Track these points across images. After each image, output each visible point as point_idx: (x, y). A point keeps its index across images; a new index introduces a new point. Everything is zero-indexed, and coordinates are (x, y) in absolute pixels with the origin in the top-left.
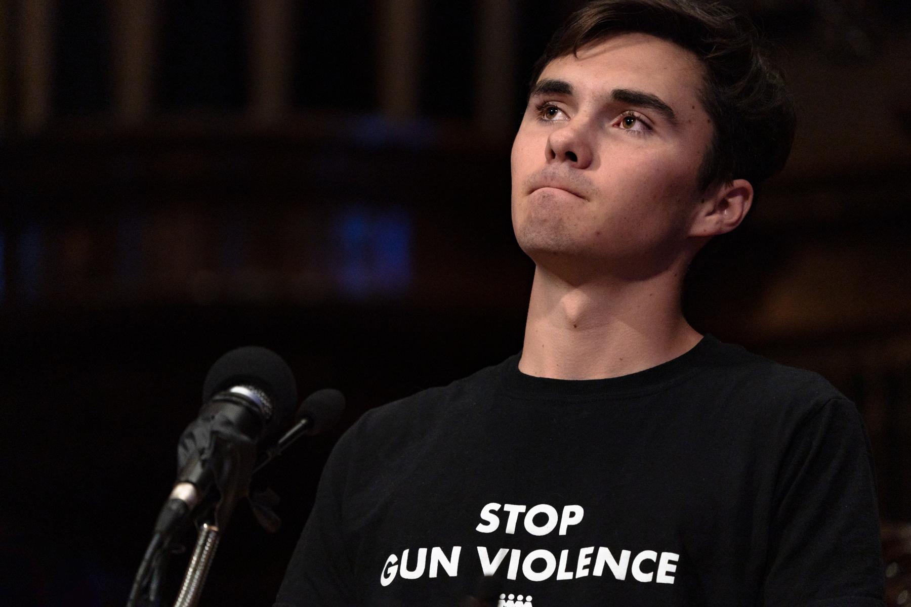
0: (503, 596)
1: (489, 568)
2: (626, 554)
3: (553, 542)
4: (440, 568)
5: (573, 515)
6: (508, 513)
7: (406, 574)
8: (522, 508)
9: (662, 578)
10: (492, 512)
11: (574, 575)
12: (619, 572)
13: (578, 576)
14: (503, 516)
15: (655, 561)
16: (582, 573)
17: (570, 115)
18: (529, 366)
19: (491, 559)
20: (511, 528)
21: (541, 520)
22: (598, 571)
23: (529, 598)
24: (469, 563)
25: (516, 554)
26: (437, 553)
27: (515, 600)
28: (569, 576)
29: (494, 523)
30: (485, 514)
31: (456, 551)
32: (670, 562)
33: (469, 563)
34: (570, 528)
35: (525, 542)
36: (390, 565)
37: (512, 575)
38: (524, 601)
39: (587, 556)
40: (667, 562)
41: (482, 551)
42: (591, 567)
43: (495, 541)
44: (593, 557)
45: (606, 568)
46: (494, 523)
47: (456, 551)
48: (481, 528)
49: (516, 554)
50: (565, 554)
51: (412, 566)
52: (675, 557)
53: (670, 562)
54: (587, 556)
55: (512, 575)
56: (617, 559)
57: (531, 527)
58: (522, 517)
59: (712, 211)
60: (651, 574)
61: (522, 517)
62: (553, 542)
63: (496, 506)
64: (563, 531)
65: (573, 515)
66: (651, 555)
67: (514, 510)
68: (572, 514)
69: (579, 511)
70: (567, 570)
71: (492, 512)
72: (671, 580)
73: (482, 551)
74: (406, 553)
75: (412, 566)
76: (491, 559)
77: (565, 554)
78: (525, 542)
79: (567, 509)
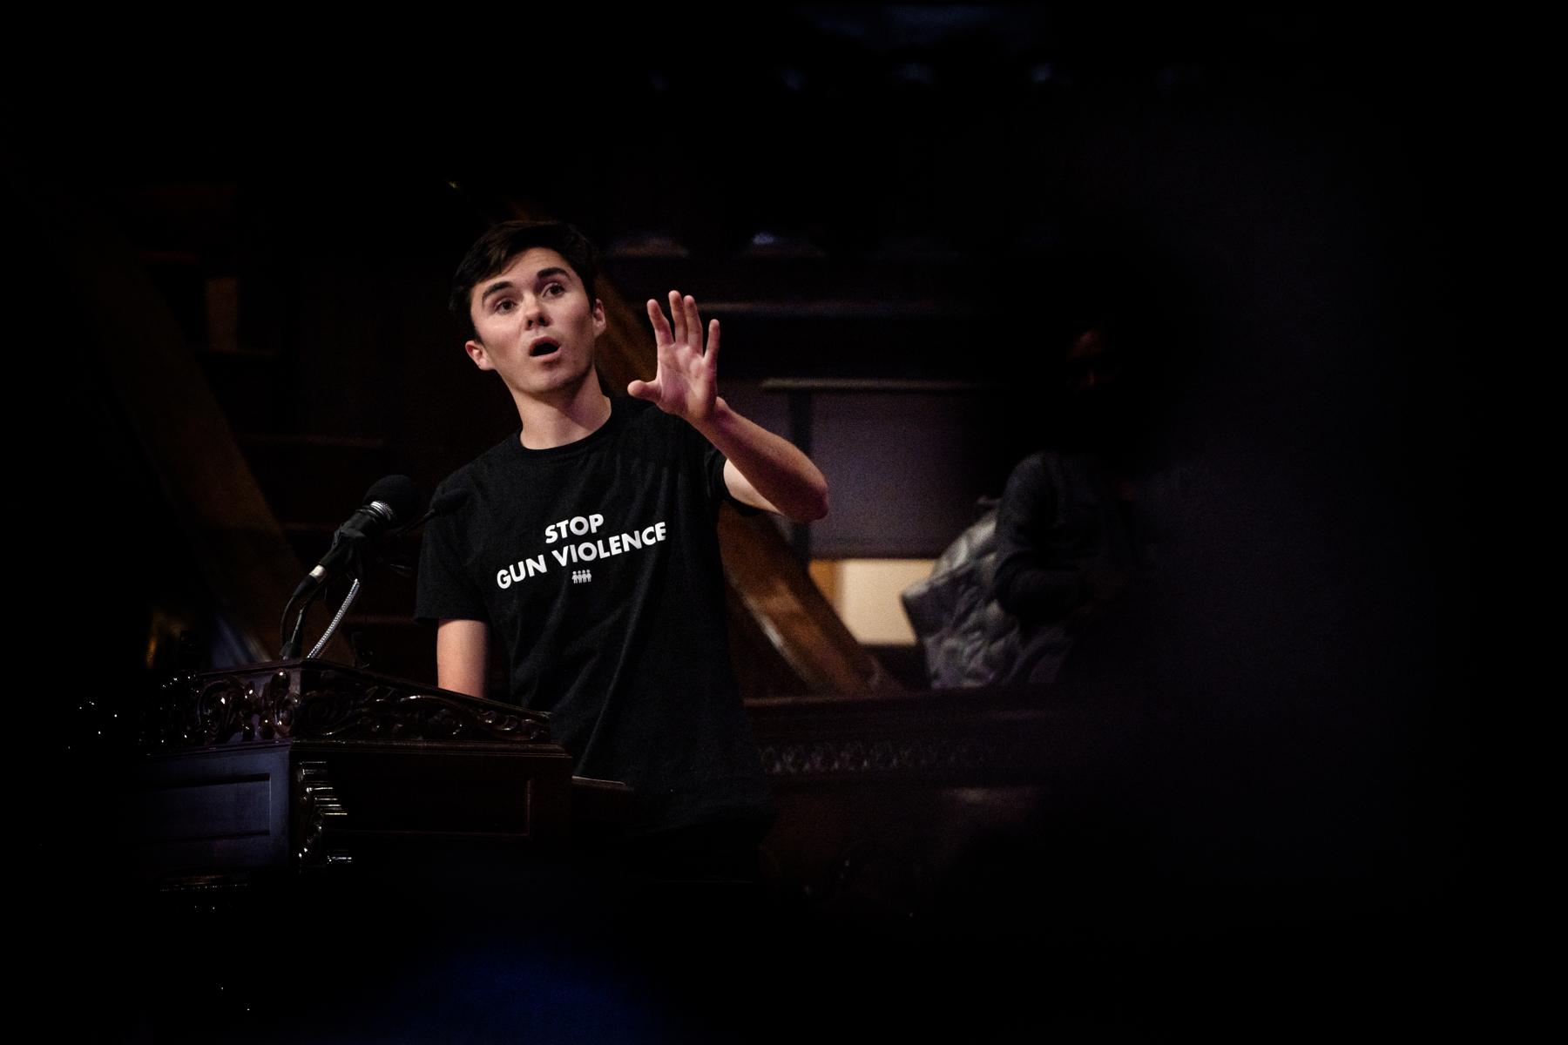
0: (574, 573)
1: (563, 561)
3: (590, 537)
4: (634, 537)
5: (597, 520)
6: (560, 528)
7: (517, 579)
8: (566, 522)
9: (660, 538)
11: (656, 539)
12: (638, 545)
14: (558, 530)
16: (615, 552)
18: (530, 441)
19: (561, 554)
20: (564, 535)
22: (627, 548)
23: (588, 571)
24: (551, 562)
25: (573, 547)
26: (530, 562)
28: (608, 554)
29: (555, 536)
30: (548, 532)
31: (541, 558)
32: (662, 528)
33: (551, 562)
34: (598, 528)
35: (574, 540)
36: (503, 576)
38: (586, 573)
39: (616, 542)
41: (555, 553)
42: (622, 547)
43: (560, 544)
44: (621, 541)
46: (555, 536)
47: (541, 558)
48: (548, 541)
50: (600, 543)
51: (518, 574)
52: (663, 524)
53: (662, 528)
54: (616, 542)
55: (575, 559)
56: (535, 569)
58: (568, 527)
60: (654, 539)
62: (590, 537)
63: (553, 527)
64: (594, 530)
65: (597, 520)
66: (650, 529)
67: (562, 525)
68: (596, 520)
70: (605, 551)
71: (551, 530)
73: (555, 553)
75: (518, 574)
76: (561, 554)
78: (574, 540)
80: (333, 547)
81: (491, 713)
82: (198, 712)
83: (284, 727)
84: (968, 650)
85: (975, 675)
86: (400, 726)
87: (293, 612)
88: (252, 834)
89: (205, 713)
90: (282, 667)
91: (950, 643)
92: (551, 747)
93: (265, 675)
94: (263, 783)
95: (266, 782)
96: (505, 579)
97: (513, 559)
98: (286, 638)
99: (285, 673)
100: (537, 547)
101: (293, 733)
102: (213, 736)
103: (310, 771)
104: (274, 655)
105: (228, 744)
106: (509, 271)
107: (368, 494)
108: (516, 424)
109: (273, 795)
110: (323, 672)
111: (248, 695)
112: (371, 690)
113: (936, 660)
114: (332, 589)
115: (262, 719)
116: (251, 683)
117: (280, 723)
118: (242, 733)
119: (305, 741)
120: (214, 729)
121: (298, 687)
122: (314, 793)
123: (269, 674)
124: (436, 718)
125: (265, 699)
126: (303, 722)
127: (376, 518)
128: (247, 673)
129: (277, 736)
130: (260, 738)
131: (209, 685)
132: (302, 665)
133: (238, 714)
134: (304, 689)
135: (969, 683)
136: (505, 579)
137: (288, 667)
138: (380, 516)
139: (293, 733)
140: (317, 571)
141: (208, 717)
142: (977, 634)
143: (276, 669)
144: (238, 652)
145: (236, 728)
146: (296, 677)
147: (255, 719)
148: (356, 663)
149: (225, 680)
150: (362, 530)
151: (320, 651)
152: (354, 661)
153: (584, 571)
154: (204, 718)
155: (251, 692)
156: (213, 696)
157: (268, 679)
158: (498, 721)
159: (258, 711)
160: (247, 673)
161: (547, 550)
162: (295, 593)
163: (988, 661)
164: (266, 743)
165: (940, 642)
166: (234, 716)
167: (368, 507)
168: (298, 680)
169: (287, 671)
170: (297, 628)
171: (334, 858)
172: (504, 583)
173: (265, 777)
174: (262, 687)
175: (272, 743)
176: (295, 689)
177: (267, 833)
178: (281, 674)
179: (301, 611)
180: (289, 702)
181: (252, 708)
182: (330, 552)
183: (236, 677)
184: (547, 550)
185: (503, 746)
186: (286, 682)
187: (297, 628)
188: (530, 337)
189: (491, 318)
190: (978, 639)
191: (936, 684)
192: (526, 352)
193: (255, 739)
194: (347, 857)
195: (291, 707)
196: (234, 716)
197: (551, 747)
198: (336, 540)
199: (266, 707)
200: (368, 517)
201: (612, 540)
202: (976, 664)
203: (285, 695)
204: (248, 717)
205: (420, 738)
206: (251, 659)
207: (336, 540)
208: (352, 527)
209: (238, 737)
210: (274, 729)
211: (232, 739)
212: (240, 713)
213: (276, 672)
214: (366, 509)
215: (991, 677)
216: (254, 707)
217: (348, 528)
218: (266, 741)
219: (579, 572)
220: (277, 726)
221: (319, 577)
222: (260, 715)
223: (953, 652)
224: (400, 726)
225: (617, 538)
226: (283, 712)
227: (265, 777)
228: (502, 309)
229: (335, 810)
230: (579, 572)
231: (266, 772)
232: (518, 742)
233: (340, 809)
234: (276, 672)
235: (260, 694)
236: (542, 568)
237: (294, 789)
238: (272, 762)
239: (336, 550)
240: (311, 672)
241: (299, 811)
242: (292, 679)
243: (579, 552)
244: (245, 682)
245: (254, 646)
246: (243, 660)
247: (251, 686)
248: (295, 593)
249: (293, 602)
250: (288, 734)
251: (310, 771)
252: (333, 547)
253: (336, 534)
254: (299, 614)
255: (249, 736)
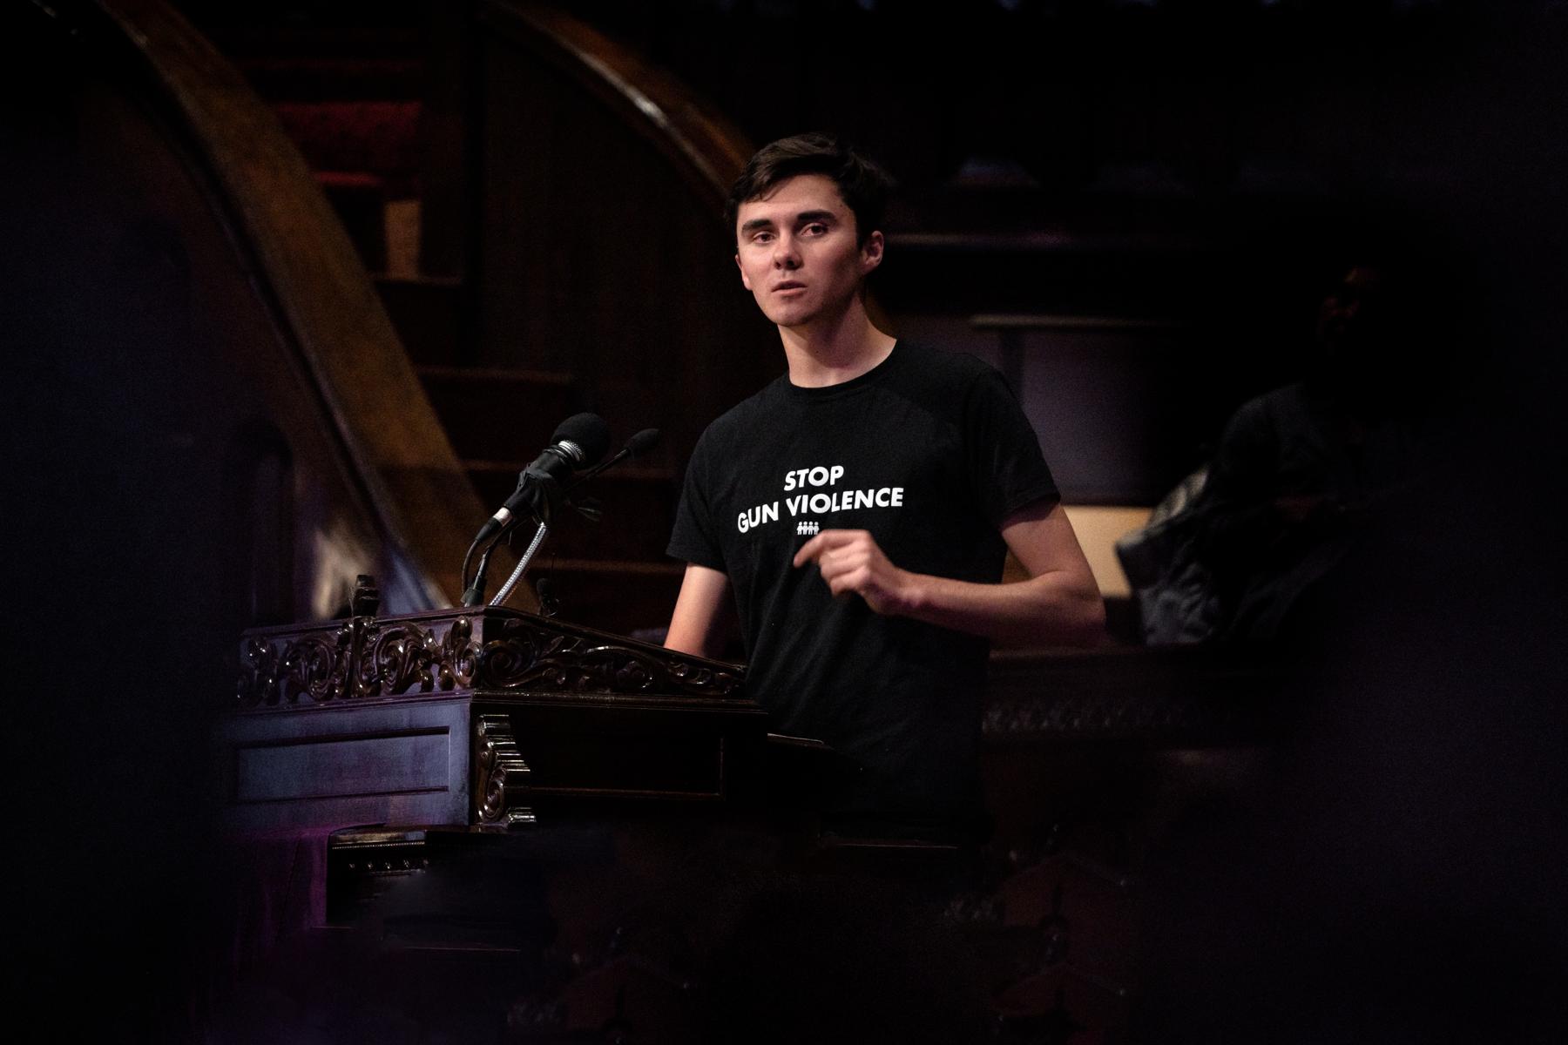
0: (800, 523)
1: (793, 512)
2: (871, 492)
3: (827, 489)
4: (769, 517)
5: (838, 472)
6: (799, 476)
8: (807, 471)
9: (895, 503)
10: (791, 477)
12: (869, 504)
13: (843, 508)
14: (797, 478)
15: (483, 617)
16: (845, 507)
17: (441, 784)
19: (793, 502)
20: (801, 484)
21: (818, 476)
22: (857, 506)
23: (816, 523)
24: (784, 510)
25: (805, 497)
26: (766, 508)
27: (808, 525)
28: (838, 508)
29: (793, 482)
30: (788, 479)
31: (776, 505)
32: (899, 493)
33: (784, 510)
34: (836, 480)
35: (810, 490)
36: (742, 520)
37: (804, 510)
38: (814, 525)
39: (849, 497)
40: (897, 494)
41: (789, 501)
43: (797, 491)
44: (854, 497)
45: (862, 503)
47: (776, 505)
49: (805, 497)
50: (835, 495)
52: (901, 490)
53: (899, 493)
54: (849, 497)
55: (804, 510)
56: (867, 496)
57: (812, 481)
58: (807, 475)
59: (795, 322)
61: (807, 475)
62: (827, 489)
64: (832, 483)
65: (838, 472)
66: (886, 490)
67: (802, 473)
68: (837, 472)
69: (841, 469)
70: (837, 505)
71: (791, 477)
72: (900, 504)
73: (789, 501)
74: (750, 511)
75: (754, 519)
76: (793, 502)
77: (835, 495)
78: (810, 490)
79: (834, 469)
80: (519, 489)
81: (682, 666)
82: (375, 660)
83: (465, 677)
84: (1186, 603)
85: (1192, 630)
86: (587, 678)
87: (475, 558)
88: (429, 790)
89: (381, 662)
90: (463, 615)
91: (1167, 595)
92: (745, 702)
93: (447, 622)
94: (443, 736)
95: (446, 735)
96: (744, 523)
97: (752, 504)
98: (467, 585)
99: (467, 620)
100: (777, 494)
101: (474, 684)
102: (391, 687)
103: (491, 725)
104: (454, 599)
105: (404, 695)
106: (771, 197)
107: (557, 433)
108: (781, 363)
109: (452, 753)
110: (508, 620)
111: (427, 643)
112: (556, 641)
113: (1153, 613)
114: (516, 533)
115: (442, 668)
116: (430, 630)
117: (461, 673)
118: (420, 684)
119: (487, 693)
120: (390, 678)
121: (481, 636)
122: (496, 748)
123: (451, 622)
124: (625, 670)
125: (446, 649)
126: (484, 673)
127: (564, 458)
128: (425, 620)
129: (457, 687)
130: (440, 689)
131: (386, 633)
132: (486, 612)
133: (416, 663)
134: (486, 639)
135: (1186, 639)
136: (744, 523)
137: (470, 615)
138: (569, 457)
139: (474, 684)
140: (502, 514)
141: (384, 666)
142: (1195, 588)
143: (457, 616)
144: (415, 595)
145: (413, 678)
146: (478, 625)
147: (435, 669)
148: (541, 612)
149: (403, 628)
150: (549, 472)
151: (503, 599)
152: (539, 609)
153: (811, 523)
154: (381, 667)
155: (430, 640)
156: (390, 644)
157: (449, 627)
158: (691, 675)
159: (438, 661)
160: (425, 620)
161: (782, 497)
162: (479, 536)
163: (1206, 616)
164: (447, 694)
165: (1156, 594)
166: (413, 665)
167: (555, 446)
168: (480, 629)
169: (469, 619)
170: (479, 573)
171: (516, 816)
172: (743, 526)
173: (444, 730)
174: (443, 635)
175: (454, 694)
176: (477, 637)
177: (444, 789)
178: (463, 622)
179: (484, 556)
180: (470, 651)
181: (430, 658)
182: (514, 494)
183: (414, 624)
184: (782, 497)
185: (695, 700)
186: (468, 631)
187: (479, 573)
188: (778, 276)
189: (749, 246)
190: (1196, 592)
191: (1151, 640)
192: (769, 288)
193: (434, 690)
194: (530, 815)
195: (472, 657)
196: (413, 665)
197: (745, 702)
198: (522, 481)
199: (446, 656)
200: (557, 457)
201: (846, 494)
202: (1194, 618)
203: (467, 644)
204: (427, 666)
205: (608, 691)
206: (429, 605)
207: (522, 481)
208: (539, 468)
209: (416, 687)
210: (455, 679)
211: (409, 691)
212: (419, 662)
213: (457, 620)
214: (553, 448)
215: (1210, 631)
216: (433, 656)
217: (534, 469)
218: (445, 692)
219: (811, 523)
220: (457, 678)
221: (504, 520)
222: (439, 664)
223: (1169, 606)
224: (587, 678)
225: (851, 493)
226: (464, 662)
227: (444, 730)
228: (760, 241)
229: (519, 766)
230: (805, 523)
231: (444, 725)
232: (711, 697)
233: (523, 765)
234: (457, 620)
235: (440, 642)
236: (775, 516)
237: (475, 743)
238: (452, 714)
239: (521, 491)
240: (494, 621)
241: (479, 769)
242: (474, 626)
243: (807, 503)
244: (424, 630)
245: (432, 591)
246: (421, 607)
247: (430, 633)
248: (479, 536)
249: (475, 548)
250: (469, 686)
251: (491, 725)
252: (519, 489)
253: (522, 475)
254: (481, 559)
255: (428, 686)
